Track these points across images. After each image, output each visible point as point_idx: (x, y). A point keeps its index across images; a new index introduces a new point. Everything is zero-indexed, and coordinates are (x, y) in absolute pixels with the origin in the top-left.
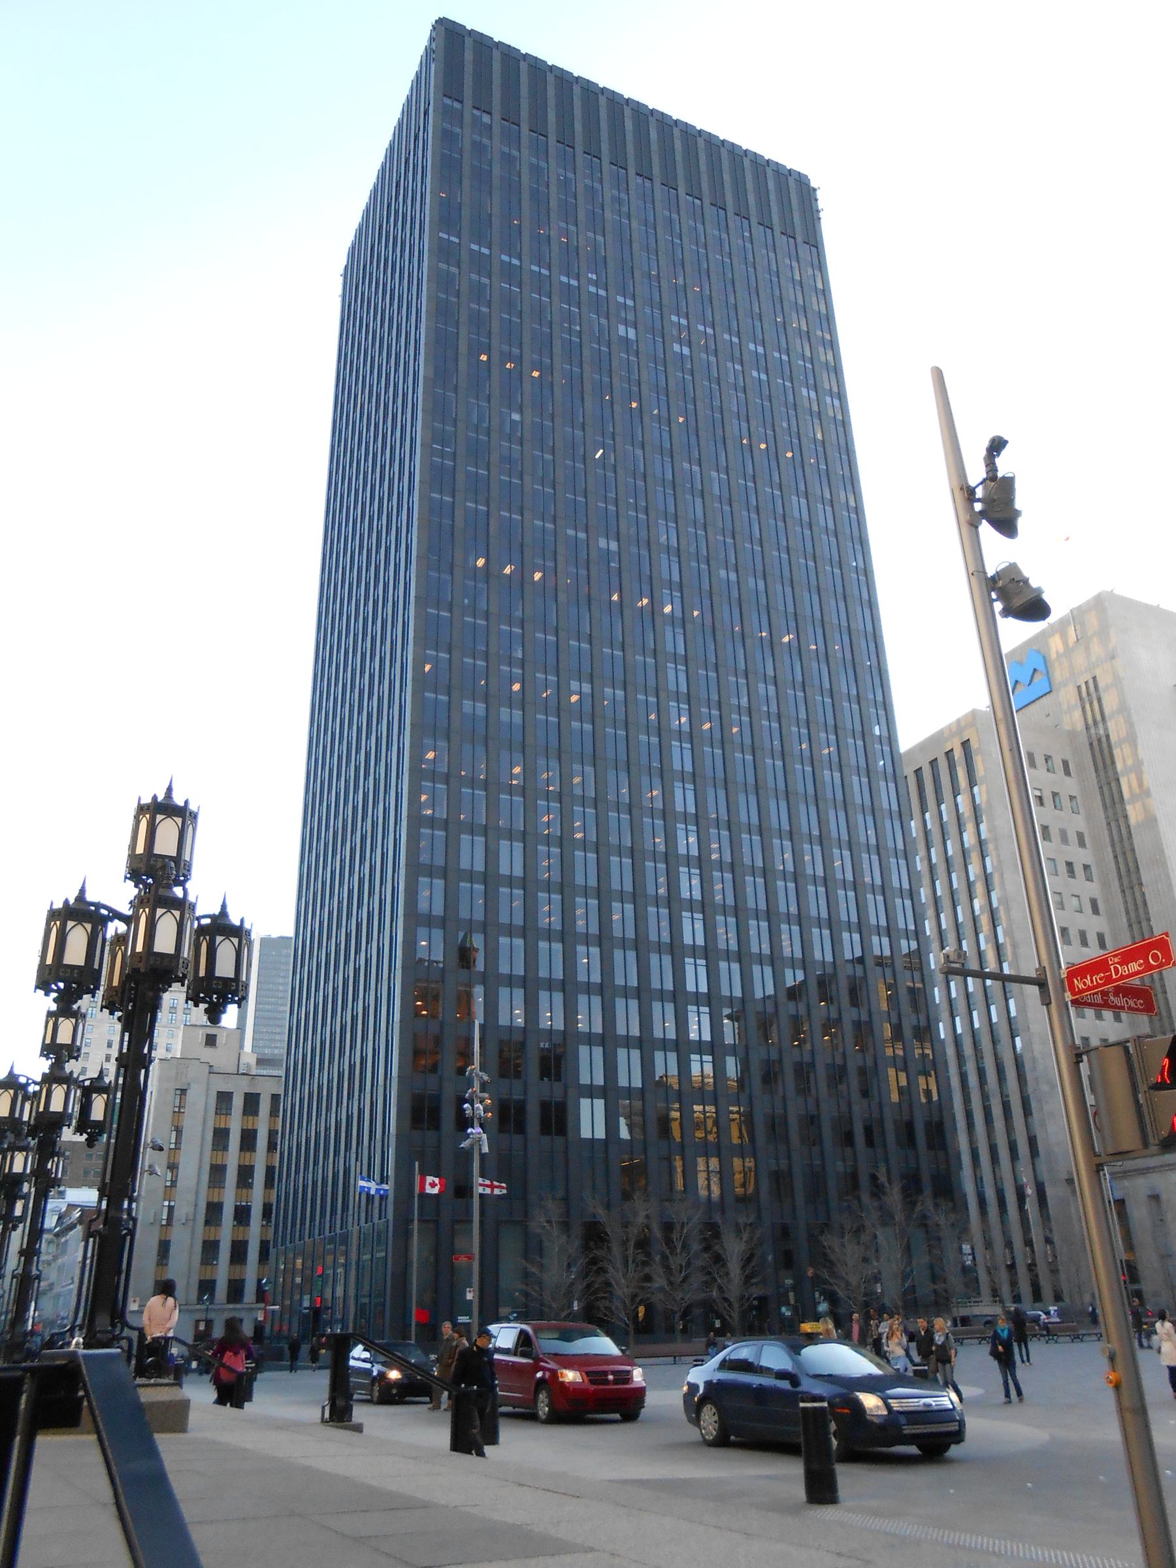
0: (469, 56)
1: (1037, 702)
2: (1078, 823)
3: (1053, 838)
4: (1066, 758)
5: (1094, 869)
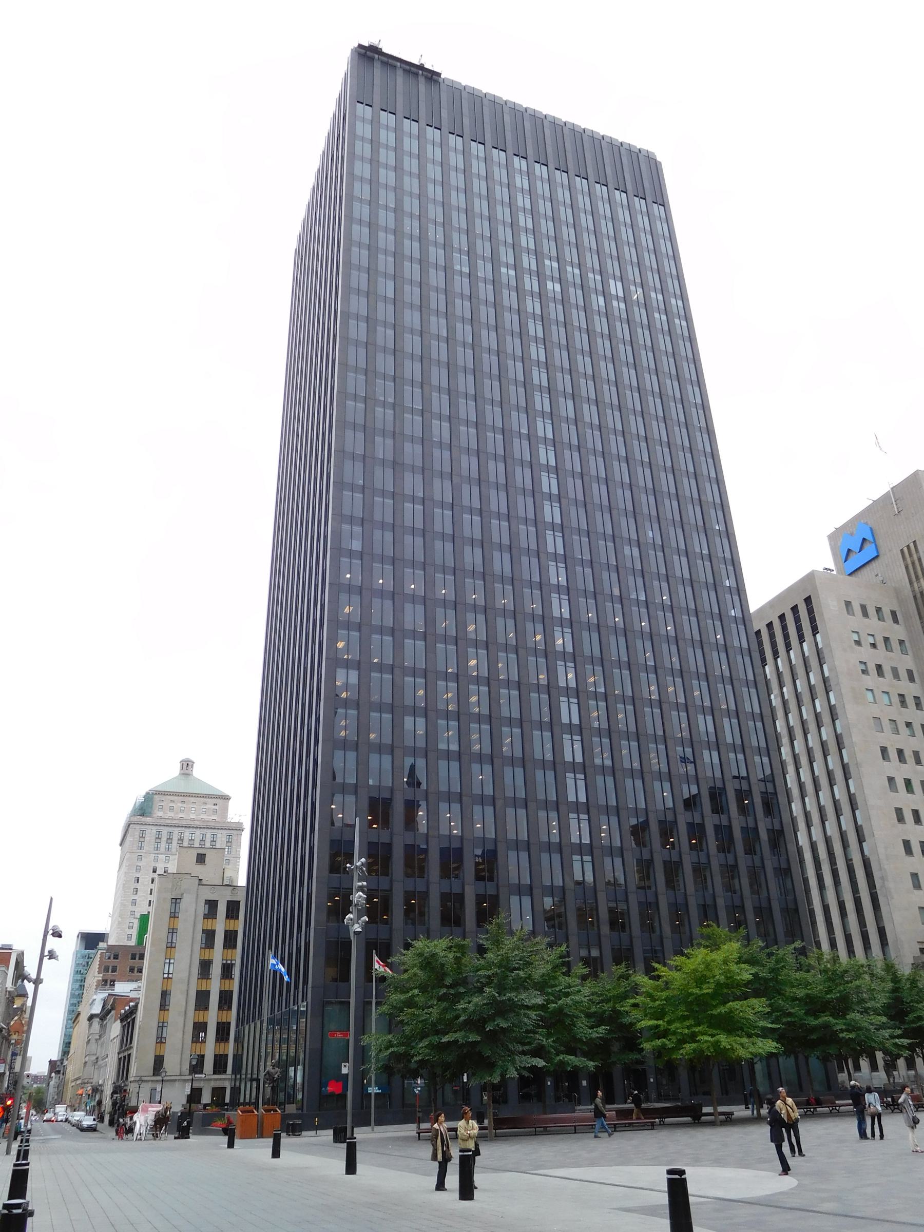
3: (886, 675)
5: (907, 644)
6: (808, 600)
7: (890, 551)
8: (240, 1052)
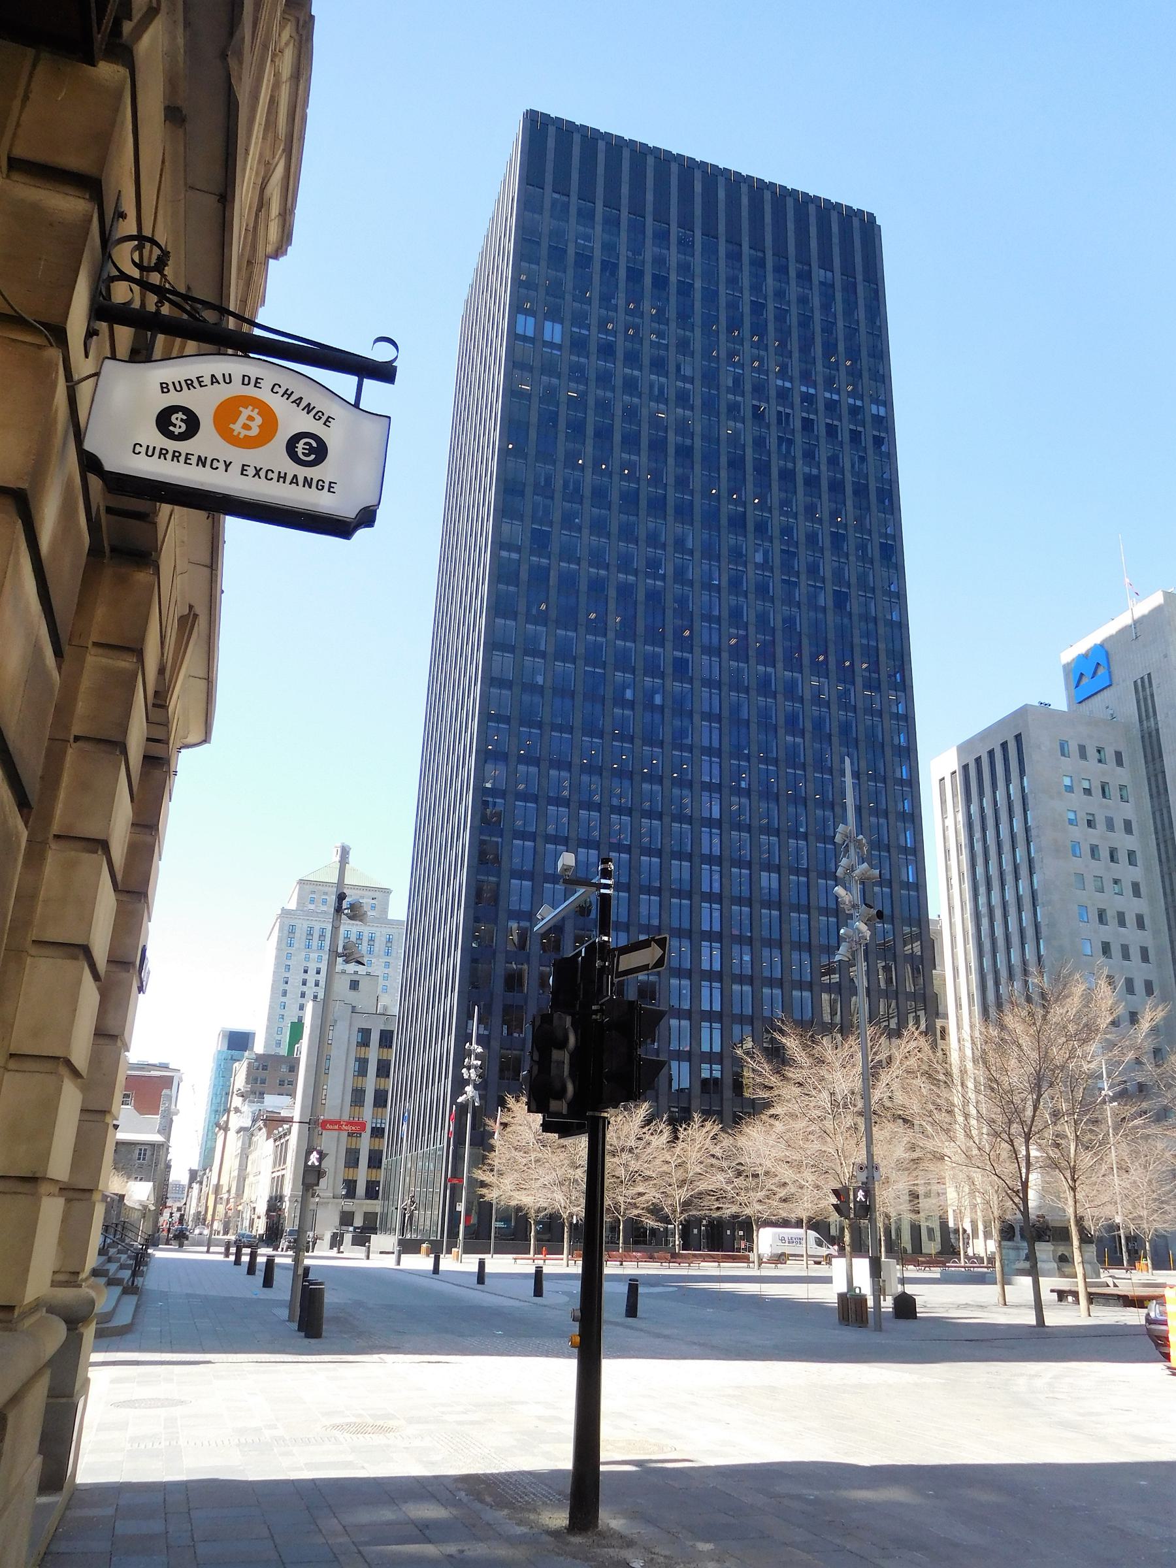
5: (1138, 854)
6: (1018, 738)
7: (1123, 681)
8: (386, 1211)
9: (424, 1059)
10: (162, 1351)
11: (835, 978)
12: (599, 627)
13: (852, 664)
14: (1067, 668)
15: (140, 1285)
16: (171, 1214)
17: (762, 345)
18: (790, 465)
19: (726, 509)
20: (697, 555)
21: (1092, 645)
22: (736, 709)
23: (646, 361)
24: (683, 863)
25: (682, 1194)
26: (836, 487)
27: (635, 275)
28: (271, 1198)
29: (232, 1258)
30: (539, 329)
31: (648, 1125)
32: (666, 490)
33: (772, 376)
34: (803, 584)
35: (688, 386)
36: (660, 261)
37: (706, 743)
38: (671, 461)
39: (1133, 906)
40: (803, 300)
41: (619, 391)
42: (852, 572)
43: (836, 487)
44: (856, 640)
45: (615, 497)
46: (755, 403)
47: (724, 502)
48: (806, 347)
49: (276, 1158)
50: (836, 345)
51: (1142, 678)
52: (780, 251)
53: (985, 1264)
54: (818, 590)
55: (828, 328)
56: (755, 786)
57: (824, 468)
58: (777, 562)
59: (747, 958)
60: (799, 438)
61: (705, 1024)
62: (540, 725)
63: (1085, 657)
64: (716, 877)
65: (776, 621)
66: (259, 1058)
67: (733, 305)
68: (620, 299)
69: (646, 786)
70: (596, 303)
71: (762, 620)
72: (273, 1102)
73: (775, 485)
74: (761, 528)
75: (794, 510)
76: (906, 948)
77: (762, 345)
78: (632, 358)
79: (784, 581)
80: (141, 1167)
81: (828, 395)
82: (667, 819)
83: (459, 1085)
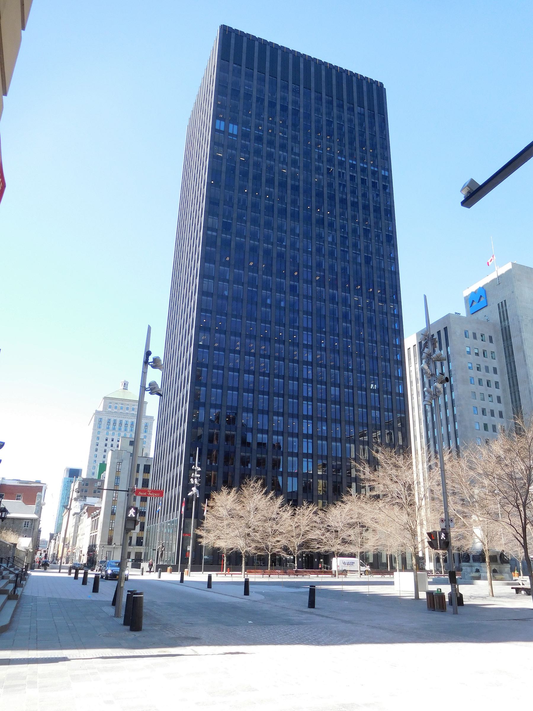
0: (245, 45)
1: (481, 310)
2: (498, 392)
4: (491, 335)
6: (446, 329)
7: (493, 304)
9: (167, 477)
10: (29, 648)
11: (366, 438)
12: (255, 269)
13: (373, 290)
14: (466, 298)
15: (19, 594)
16: (41, 554)
17: (331, 140)
18: (344, 197)
19: (315, 216)
20: (301, 236)
21: (478, 287)
22: (319, 310)
23: (277, 145)
24: (294, 382)
25: (298, 541)
26: (366, 207)
27: (272, 104)
28: (90, 546)
29: (73, 575)
30: (227, 127)
31: (282, 507)
32: (286, 206)
33: (336, 155)
34: (351, 253)
35: (297, 157)
36: (284, 99)
37: (305, 325)
38: (289, 192)
39: (498, 407)
40: (350, 121)
41: (264, 158)
42: (373, 248)
43: (366, 207)
44: (375, 279)
45: (262, 208)
46: (328, 167)
47: (313, 212)
48: (352, 142)
49: (92, 526)
50: (366, 142)
51: (502, 302)
52: (340, 98)
53: (443, 574)
54: (358, 255)
55: (362, 134)
56: (328, 347)
57: (360, 198)
58: (339, 242)
59: (324, 428)
60: (348, 184)
61: (305, 459)
62: (226, 315)
63: (475, 293)
64: (310, 389)
65: (338, 268)
66: (84, 480)
67: (318, 121)
68: (265, 115)
69: (277, 345)
70: (253, 116)
71: (332, 268)
72: (90, 500)
73: (338, 206)
74: (331, 225)
75: (346, 217)
76: (398, 424)
77: (331, 140)
78: (271, 143)
79: (341, 250)
80: (26, 530)
81: (362, 165)
82: (287, 361)
83: (187, 487)
